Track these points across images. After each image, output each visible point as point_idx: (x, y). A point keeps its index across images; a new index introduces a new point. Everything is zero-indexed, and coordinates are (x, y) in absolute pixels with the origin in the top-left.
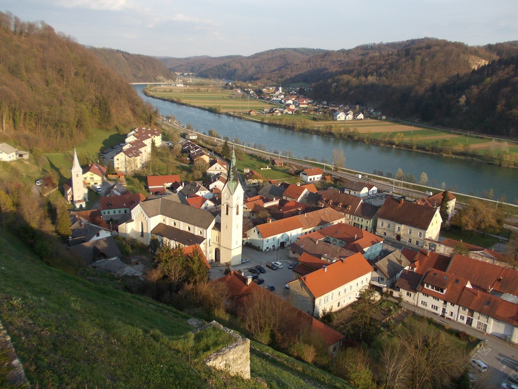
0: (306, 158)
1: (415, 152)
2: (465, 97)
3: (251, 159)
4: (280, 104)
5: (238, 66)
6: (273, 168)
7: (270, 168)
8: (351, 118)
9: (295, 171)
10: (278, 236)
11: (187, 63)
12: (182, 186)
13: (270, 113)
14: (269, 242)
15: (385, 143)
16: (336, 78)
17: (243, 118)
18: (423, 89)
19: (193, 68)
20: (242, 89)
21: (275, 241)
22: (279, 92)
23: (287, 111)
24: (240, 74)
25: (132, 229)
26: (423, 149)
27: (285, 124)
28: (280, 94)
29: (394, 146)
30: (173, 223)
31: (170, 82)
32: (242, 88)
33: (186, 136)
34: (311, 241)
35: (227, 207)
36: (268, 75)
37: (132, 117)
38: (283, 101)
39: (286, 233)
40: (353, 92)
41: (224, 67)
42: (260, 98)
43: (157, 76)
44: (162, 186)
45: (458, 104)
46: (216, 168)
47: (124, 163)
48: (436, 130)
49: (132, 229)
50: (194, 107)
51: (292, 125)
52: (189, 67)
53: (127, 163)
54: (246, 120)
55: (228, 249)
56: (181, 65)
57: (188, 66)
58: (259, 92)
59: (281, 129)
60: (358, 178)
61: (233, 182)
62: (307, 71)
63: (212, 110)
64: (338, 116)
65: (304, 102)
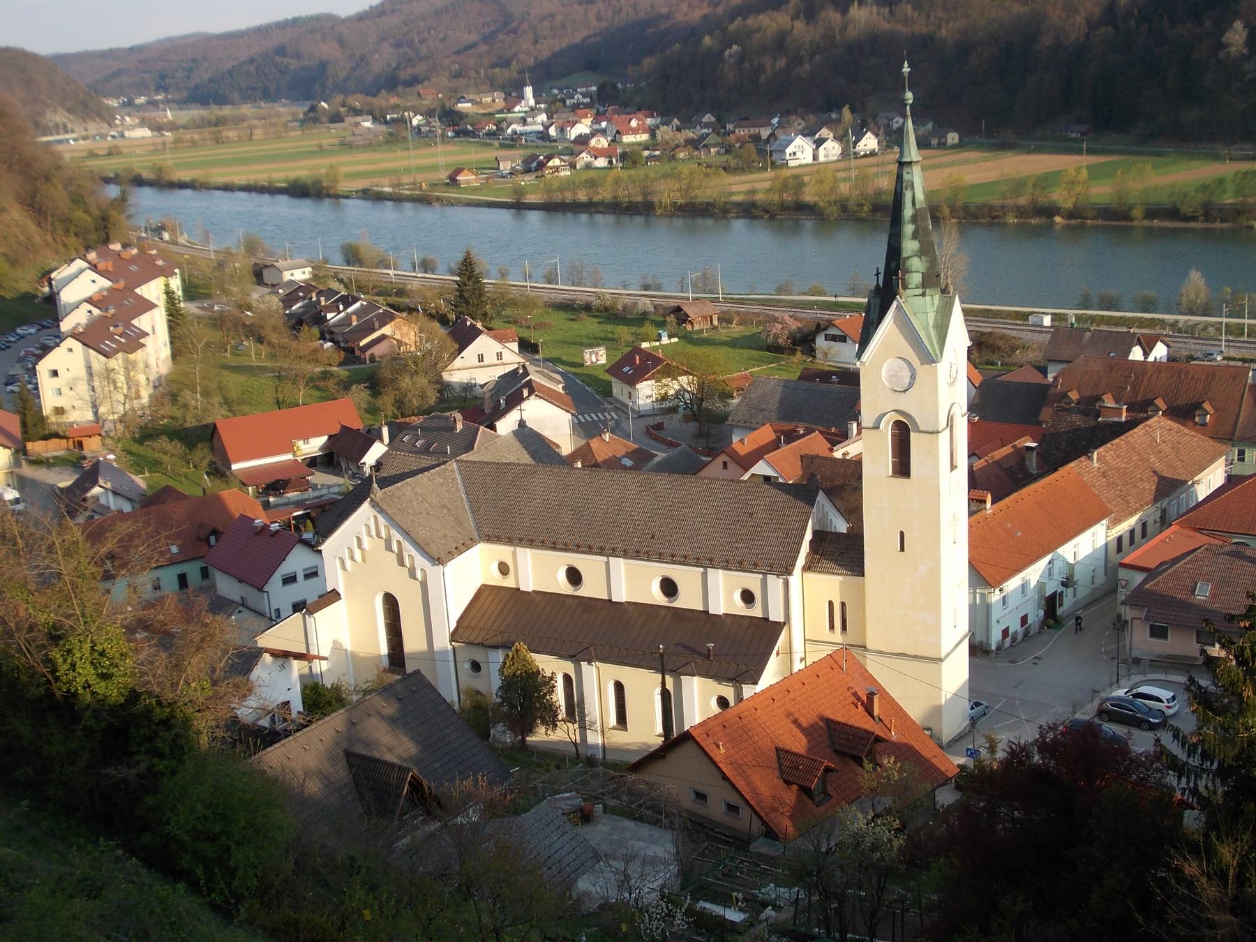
0: (780, 290)
1: (1142, 227)
2: (1245, 27)
3: (572, 320)
4: (540, 143)
5: (328, 50)
6: (687, 338)
7: (675, 340)
8: (834, 152)
9: (791, 336)
10: (1034, 573)
11: (140, 62)
12: (381, 440)
13: (528, 171)
14: (1012, 604)
15: (1021, 212)
16: (732, 28)
17: (438, 199)
18: (1079, 19)
19: (162, 77)
20: (378, 118)
21: (1030, 594)
22: (527, 105)
23: (589, 159)
24: (342, 75)
25: (335, 642)
26: (1173, 213)
27: (615, 197)
28: (533, 111)
29: (1058, 219)
30: (562, 575)
31: (93, 128)
32: (377, 113)
33: (265, 273)
34: (1238, 561)
35: (902, 434)
36: (454, 63)
37: (32, 227)
38: (552, 131)
39: (1060, 550)
40: (808, 67)
41: (278, 59)
42: (458, 134)
43: (42, 114)
44: (289, 457)
45: (1222, 55)
46: (481, 358)
47: (83, 388)
48: (1159, 154)
49: (335, 642)
50: (227, 188)
51: (640, 199)
52: (147, 75)
53: (96, 383)
54: (452, 205)
55: (916, 657)
56: (119, 73)
57: (144, 72)
58: (451, 117)
59: (599, 218)
60: (1042, 326)
61: (923, 295)
62: (591, 32)
63: (299, 191)
64: (789, 150)
65: (634, 123)
